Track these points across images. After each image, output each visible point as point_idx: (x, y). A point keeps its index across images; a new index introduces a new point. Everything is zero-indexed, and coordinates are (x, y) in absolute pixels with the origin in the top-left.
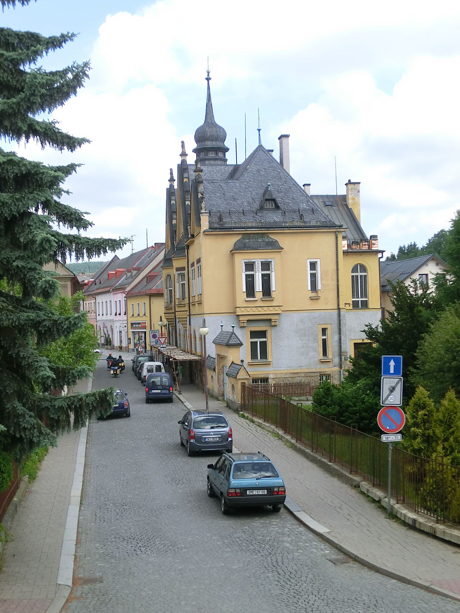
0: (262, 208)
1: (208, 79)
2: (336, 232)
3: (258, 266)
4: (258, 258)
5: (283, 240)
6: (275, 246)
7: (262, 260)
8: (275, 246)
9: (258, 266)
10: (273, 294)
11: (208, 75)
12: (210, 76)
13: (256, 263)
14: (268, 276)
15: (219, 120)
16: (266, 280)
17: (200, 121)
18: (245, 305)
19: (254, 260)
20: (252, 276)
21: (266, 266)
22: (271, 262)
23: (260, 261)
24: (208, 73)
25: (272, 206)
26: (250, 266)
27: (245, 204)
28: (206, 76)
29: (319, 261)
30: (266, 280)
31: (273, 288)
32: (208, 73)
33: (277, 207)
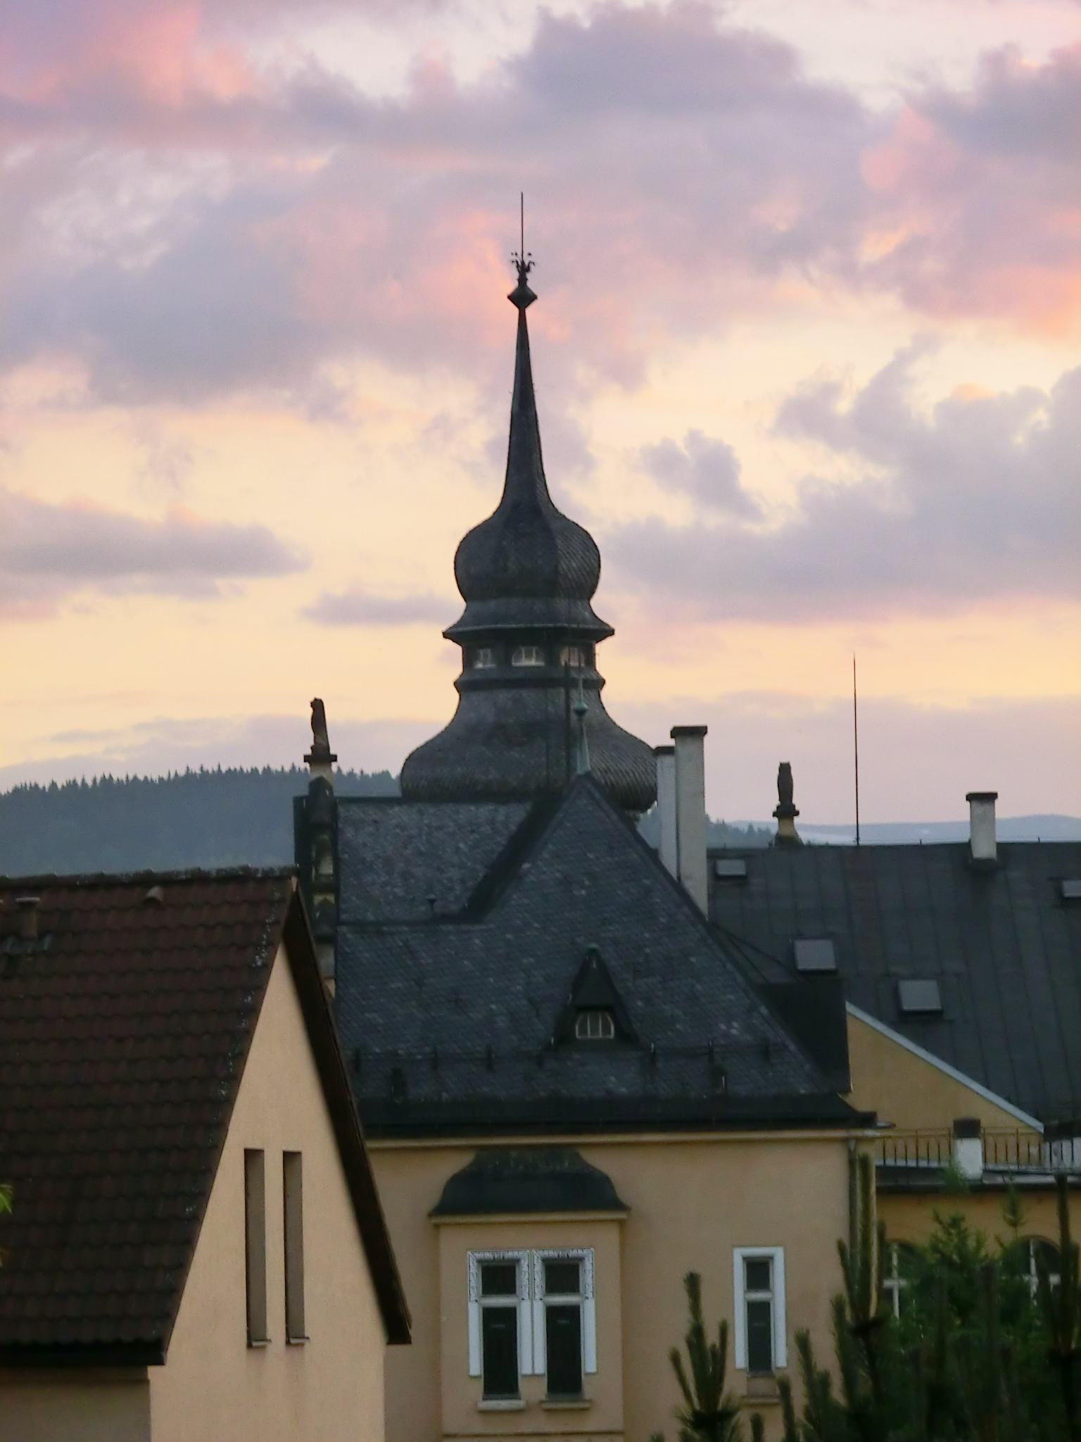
0: (564, 1038)
1: (522, 298)
2: (845, 1141)
3: (531, 1276)
4: (529, 1246)
5: (644, 1171)
6: (591, 1195)
7: (546, 1253)
8: (591, 1195)
9: (531, 1276)
10: (589, 1389)
11: (522, 280)
12: (533, 284)
13: (524, 1264)
14: (573, 1313)
15: (572, 493)
16: (563, 1330)
17: (482, 499)
18: (478, 1426)
19: (515, 1254)
20: (509, 1316)
21: (562, 1275)
22: (581, 1259)
23: (538, 1256)
24: (523, 269)
25: (606, 1029)
26: (499, 1277)
27: (502, 1022)
28: (512, 285)
29: (779, 1254)
30: (563, 1330)
31: (590, 1363)
32: (523, 269)
33: (626, 1037)
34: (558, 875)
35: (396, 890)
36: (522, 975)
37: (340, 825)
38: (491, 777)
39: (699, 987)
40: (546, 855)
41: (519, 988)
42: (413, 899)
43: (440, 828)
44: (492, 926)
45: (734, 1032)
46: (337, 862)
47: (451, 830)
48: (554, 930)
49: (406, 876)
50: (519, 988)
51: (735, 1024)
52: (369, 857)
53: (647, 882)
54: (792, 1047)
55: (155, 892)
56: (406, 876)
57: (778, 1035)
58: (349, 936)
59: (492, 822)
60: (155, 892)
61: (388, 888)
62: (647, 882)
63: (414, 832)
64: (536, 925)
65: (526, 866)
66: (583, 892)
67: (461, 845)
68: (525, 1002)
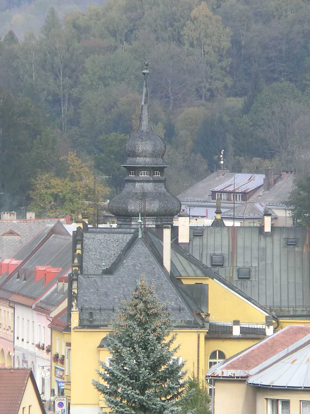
2: (198, 332)
34: (132, 263)
35: (98, 256)
36: (122, 289)
37: (84, 239)
38: (132, 208)
39: (165, 293)
40: (130, 258)
41: (121, 292)
42: (102, 259)
43: (110, 240)
44: (116, 276)
45: (172, 304)
46: (82, 249)
47: (112, 241)
48: (131, 277)
49: (100, 253)
50: (121, 292)
51: (173, 302)
52: (91, 247)
53: (153, 266)
54: (186, 308)
55: (12, 371)
56: (100, 253)
57: (183, 305)
58: (81, 278)
59: (123, 239)
60: (12, 371)
61: (95, 256)
62: (153, 266)
63: (103, 241)
64: (126, 276)
65: (125, 261)
66: (138, 268)
67: (114, 245)
68: (122, 295)
